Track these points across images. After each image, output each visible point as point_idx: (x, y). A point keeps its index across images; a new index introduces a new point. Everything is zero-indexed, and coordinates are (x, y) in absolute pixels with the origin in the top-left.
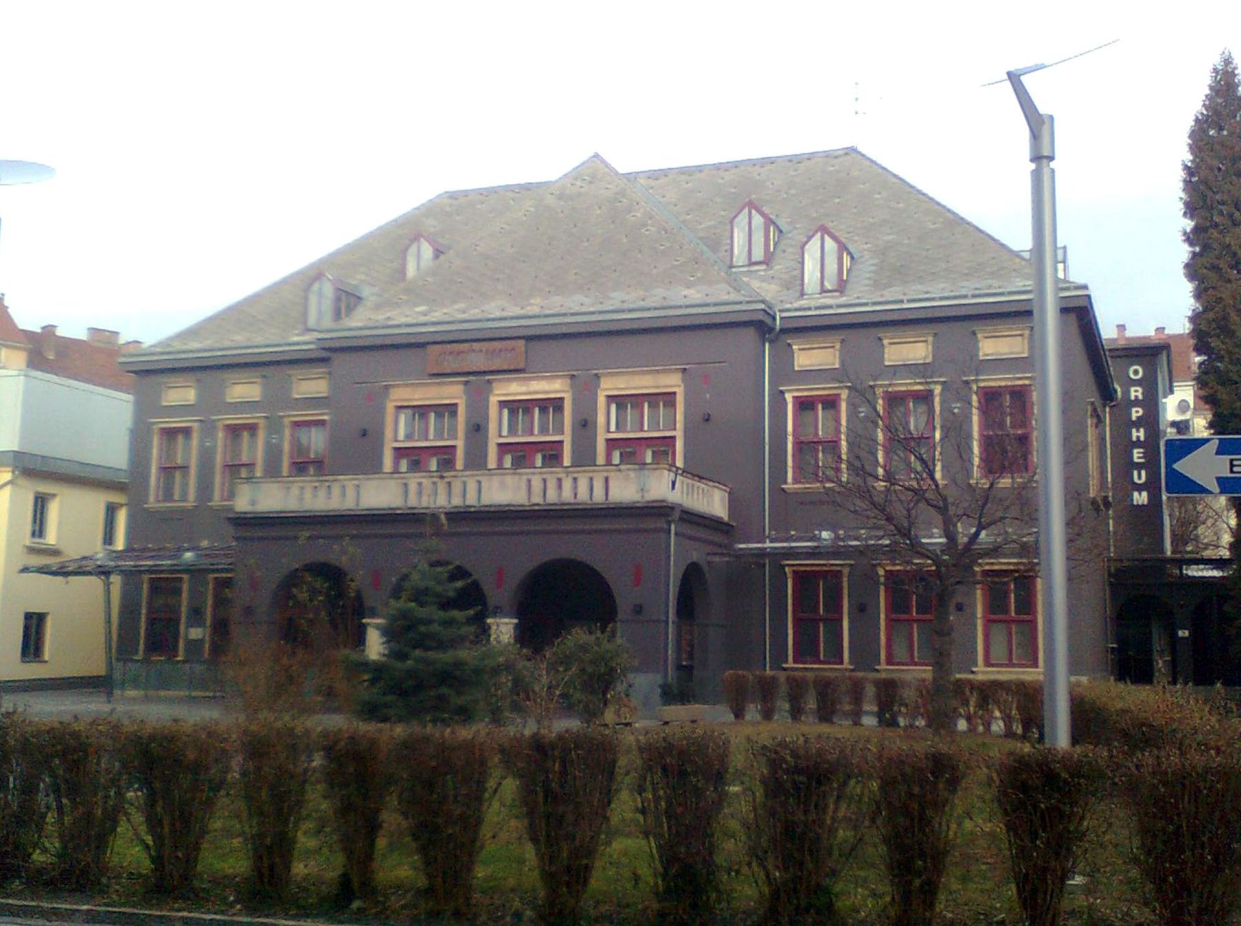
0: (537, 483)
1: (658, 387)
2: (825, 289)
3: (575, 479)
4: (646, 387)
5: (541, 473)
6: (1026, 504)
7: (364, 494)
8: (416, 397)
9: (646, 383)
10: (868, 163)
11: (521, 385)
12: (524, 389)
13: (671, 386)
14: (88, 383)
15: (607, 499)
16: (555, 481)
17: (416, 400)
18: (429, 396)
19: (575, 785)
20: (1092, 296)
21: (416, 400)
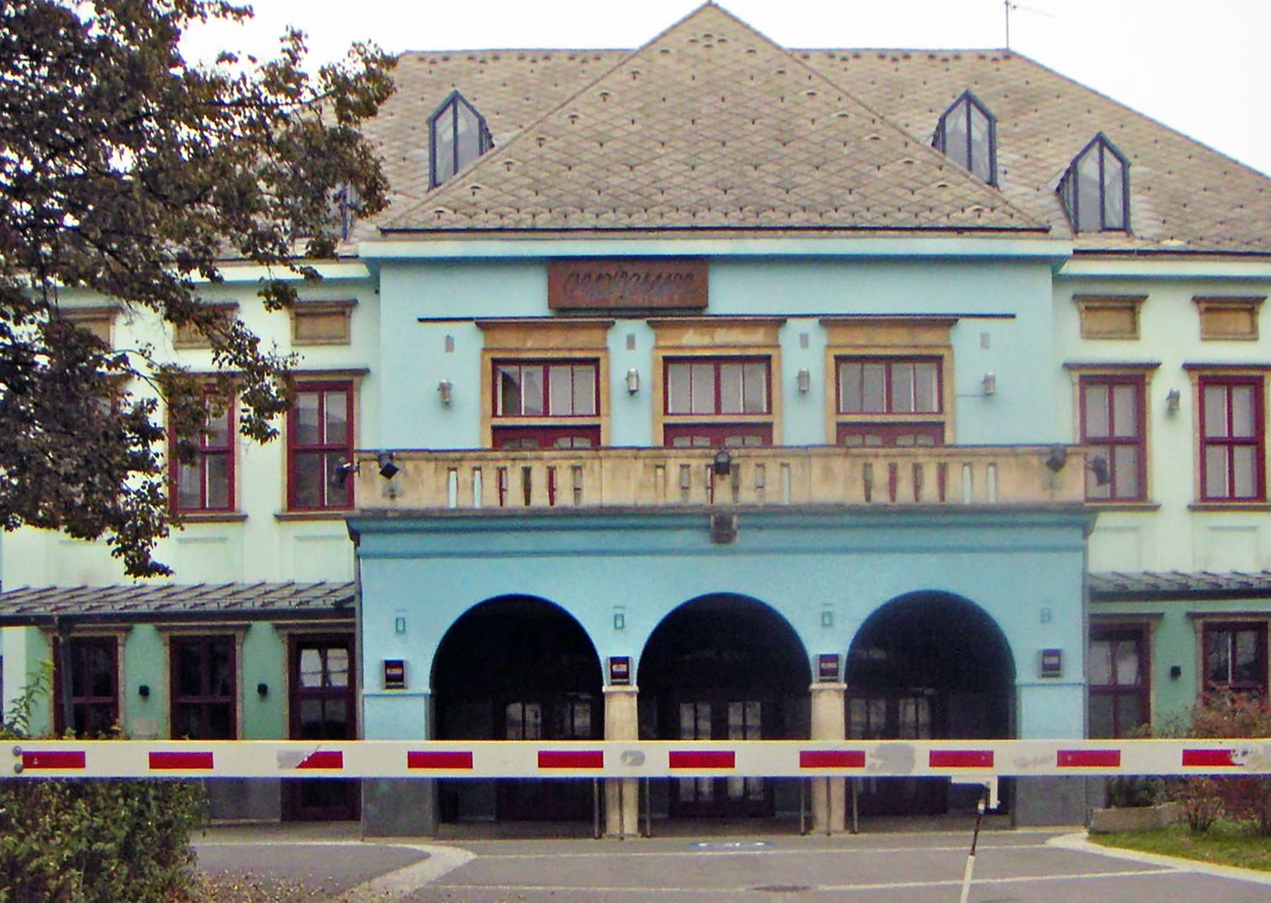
0: (880, 474)
1: (916, 347)
2: (1108, 225)
3: (501, 471)
4: (898, 346)
5: (887, 456)
6: (759, 487)
7: (587, 482)
8: (529, 344)
9: (896, 341)
10: (1067, 84)
11: (703, 335)
12: (706, 340)
13: (937, 346)
14: (1189, 874)
15: (942, 498)
16: (909, 468)
17: (529, 350)
18: (551, 345)
19: (696, 719)
20: (979, 344)
21: (529, 350)
